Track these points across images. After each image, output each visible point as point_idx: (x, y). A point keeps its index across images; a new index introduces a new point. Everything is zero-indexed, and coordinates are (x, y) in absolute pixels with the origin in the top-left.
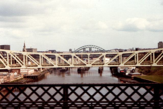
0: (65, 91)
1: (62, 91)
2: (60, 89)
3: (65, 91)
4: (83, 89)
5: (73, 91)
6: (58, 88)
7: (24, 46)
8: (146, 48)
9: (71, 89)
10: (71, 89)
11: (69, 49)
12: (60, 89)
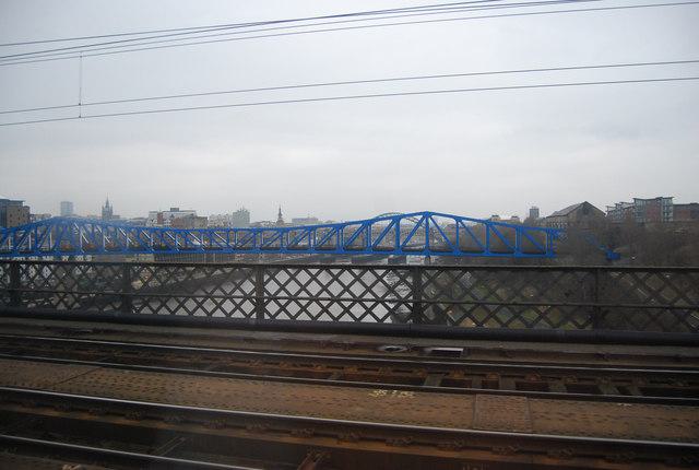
4: (310, 274)
7: (280, 215)
8: (351, 220)
11: (538, 206)
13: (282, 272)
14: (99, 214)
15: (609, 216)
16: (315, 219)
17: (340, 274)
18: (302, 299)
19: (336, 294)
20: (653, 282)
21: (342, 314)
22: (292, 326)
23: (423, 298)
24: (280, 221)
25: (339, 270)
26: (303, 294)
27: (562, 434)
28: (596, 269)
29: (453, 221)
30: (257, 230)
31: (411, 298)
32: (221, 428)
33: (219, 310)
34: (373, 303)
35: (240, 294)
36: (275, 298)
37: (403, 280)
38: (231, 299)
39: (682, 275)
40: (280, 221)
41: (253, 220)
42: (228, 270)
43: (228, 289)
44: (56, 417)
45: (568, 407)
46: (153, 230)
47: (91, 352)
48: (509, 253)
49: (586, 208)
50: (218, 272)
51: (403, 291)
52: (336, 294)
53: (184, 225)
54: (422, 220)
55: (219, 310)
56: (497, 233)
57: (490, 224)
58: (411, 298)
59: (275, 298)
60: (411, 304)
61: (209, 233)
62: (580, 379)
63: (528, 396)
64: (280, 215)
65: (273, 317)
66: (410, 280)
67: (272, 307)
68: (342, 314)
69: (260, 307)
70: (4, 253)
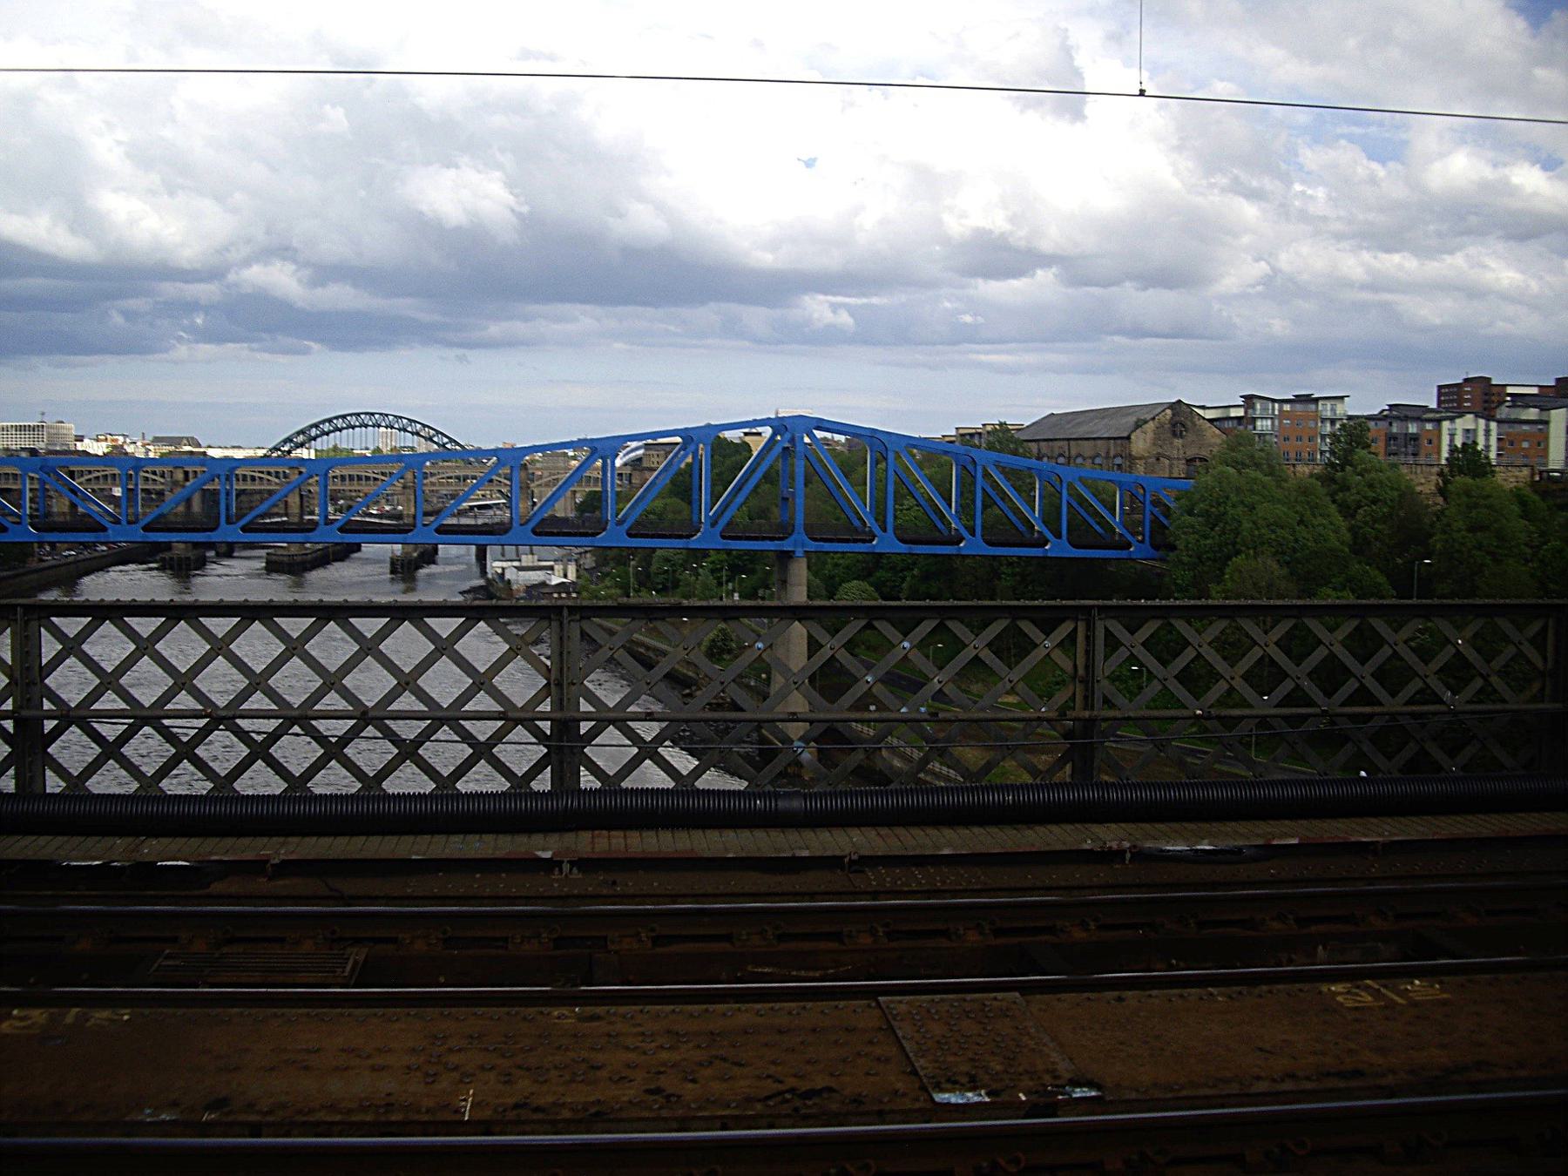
3: (1084, 774)
4: (206, 634)
5: (73, 647)
9: (58, 634)
10: (58, 634)
17: (383, 634)
18: (195, 715)
19: (147, 697)
21: (634, 763)
22: (149, 813)
23: (585, 706)
26: (110, 702)
27: (881, 1116)
28: (16, 606)
31: (546, 707)
33: (482, 766)
34: (273, 724)
35: (268, 705)
36: (511, 717)
38: (621, 723)
43: (1265, 704)
51: (520, 684)
52: (147, 697)
53: (1001, 437)
55: (482, 766)
58: (546, 707)
59: (79, 717)
60: (546, 726)
65: (76, 783)
67: (72, 749)
68: (634, 763)
69: (565, 746)
70: (1561, 507)
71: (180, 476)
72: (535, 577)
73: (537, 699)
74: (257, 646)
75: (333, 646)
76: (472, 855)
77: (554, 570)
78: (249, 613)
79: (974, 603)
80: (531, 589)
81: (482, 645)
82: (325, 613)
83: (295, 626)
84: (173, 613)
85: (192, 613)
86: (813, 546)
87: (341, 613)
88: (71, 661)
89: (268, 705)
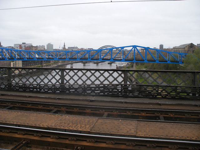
0: (62, 73)
1: (60, 73)
2: (59, 72)
3: (62, 73)
4: (91, 72)
5: (67, 73)
6: (57, 71)
7: (64, 46)
9: (66, 72)
10: (66, 72)
11: (162, 44)
12: (59, 72)
13: (54, 71)
14: (158, 47)
15: (68, 49)
16: (77, 48)
17: (69, 72)
20: (155, 76)
24: (64, 48)
25: (77, 71)
28: (195, 72)
29: (183, 49)
30: (57, 51)
32: (9, 133)
35: (15, 82)
37: (120, 75)
39: (184, 74)
40: (64, 48)
41: (54, 48)
42: (34, 70)
44: (37, 140)
45: (108, 121)
46: (17, 51)
47: (115, 113)
48: (166, 62)
49: (192, 45)
50: (31, 71)
53: (29, 49)
54: (135, 49)
56: (150, 53)
57: (82, 49)
61: (39, 53)
62: (79, 110)
63: (138, 121)
64: (64, 46)
66: (123, 75)
71: (84, 53)
72: (120, 65)
73: (122, 82)
74: (80, 74)
75: (88, 74)
76: (139, 102)
77: (124, 64)
78: (79, 70)
79: (170, 71)
80: (119, 67)
81: (115, 75)
82: (88, 70)
83: (84, 71)
84: (96, 70)
85: (98, 70)
86: (136, 61)
87: (89, 70)
88: (84, 76)
89: (15, 82)
